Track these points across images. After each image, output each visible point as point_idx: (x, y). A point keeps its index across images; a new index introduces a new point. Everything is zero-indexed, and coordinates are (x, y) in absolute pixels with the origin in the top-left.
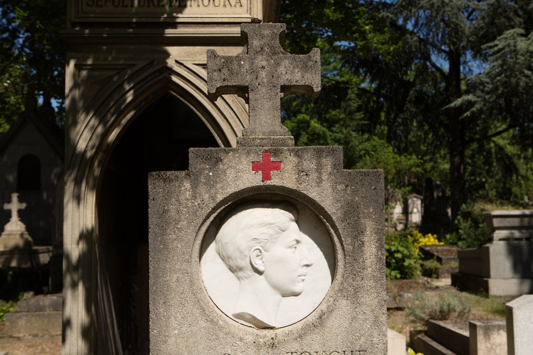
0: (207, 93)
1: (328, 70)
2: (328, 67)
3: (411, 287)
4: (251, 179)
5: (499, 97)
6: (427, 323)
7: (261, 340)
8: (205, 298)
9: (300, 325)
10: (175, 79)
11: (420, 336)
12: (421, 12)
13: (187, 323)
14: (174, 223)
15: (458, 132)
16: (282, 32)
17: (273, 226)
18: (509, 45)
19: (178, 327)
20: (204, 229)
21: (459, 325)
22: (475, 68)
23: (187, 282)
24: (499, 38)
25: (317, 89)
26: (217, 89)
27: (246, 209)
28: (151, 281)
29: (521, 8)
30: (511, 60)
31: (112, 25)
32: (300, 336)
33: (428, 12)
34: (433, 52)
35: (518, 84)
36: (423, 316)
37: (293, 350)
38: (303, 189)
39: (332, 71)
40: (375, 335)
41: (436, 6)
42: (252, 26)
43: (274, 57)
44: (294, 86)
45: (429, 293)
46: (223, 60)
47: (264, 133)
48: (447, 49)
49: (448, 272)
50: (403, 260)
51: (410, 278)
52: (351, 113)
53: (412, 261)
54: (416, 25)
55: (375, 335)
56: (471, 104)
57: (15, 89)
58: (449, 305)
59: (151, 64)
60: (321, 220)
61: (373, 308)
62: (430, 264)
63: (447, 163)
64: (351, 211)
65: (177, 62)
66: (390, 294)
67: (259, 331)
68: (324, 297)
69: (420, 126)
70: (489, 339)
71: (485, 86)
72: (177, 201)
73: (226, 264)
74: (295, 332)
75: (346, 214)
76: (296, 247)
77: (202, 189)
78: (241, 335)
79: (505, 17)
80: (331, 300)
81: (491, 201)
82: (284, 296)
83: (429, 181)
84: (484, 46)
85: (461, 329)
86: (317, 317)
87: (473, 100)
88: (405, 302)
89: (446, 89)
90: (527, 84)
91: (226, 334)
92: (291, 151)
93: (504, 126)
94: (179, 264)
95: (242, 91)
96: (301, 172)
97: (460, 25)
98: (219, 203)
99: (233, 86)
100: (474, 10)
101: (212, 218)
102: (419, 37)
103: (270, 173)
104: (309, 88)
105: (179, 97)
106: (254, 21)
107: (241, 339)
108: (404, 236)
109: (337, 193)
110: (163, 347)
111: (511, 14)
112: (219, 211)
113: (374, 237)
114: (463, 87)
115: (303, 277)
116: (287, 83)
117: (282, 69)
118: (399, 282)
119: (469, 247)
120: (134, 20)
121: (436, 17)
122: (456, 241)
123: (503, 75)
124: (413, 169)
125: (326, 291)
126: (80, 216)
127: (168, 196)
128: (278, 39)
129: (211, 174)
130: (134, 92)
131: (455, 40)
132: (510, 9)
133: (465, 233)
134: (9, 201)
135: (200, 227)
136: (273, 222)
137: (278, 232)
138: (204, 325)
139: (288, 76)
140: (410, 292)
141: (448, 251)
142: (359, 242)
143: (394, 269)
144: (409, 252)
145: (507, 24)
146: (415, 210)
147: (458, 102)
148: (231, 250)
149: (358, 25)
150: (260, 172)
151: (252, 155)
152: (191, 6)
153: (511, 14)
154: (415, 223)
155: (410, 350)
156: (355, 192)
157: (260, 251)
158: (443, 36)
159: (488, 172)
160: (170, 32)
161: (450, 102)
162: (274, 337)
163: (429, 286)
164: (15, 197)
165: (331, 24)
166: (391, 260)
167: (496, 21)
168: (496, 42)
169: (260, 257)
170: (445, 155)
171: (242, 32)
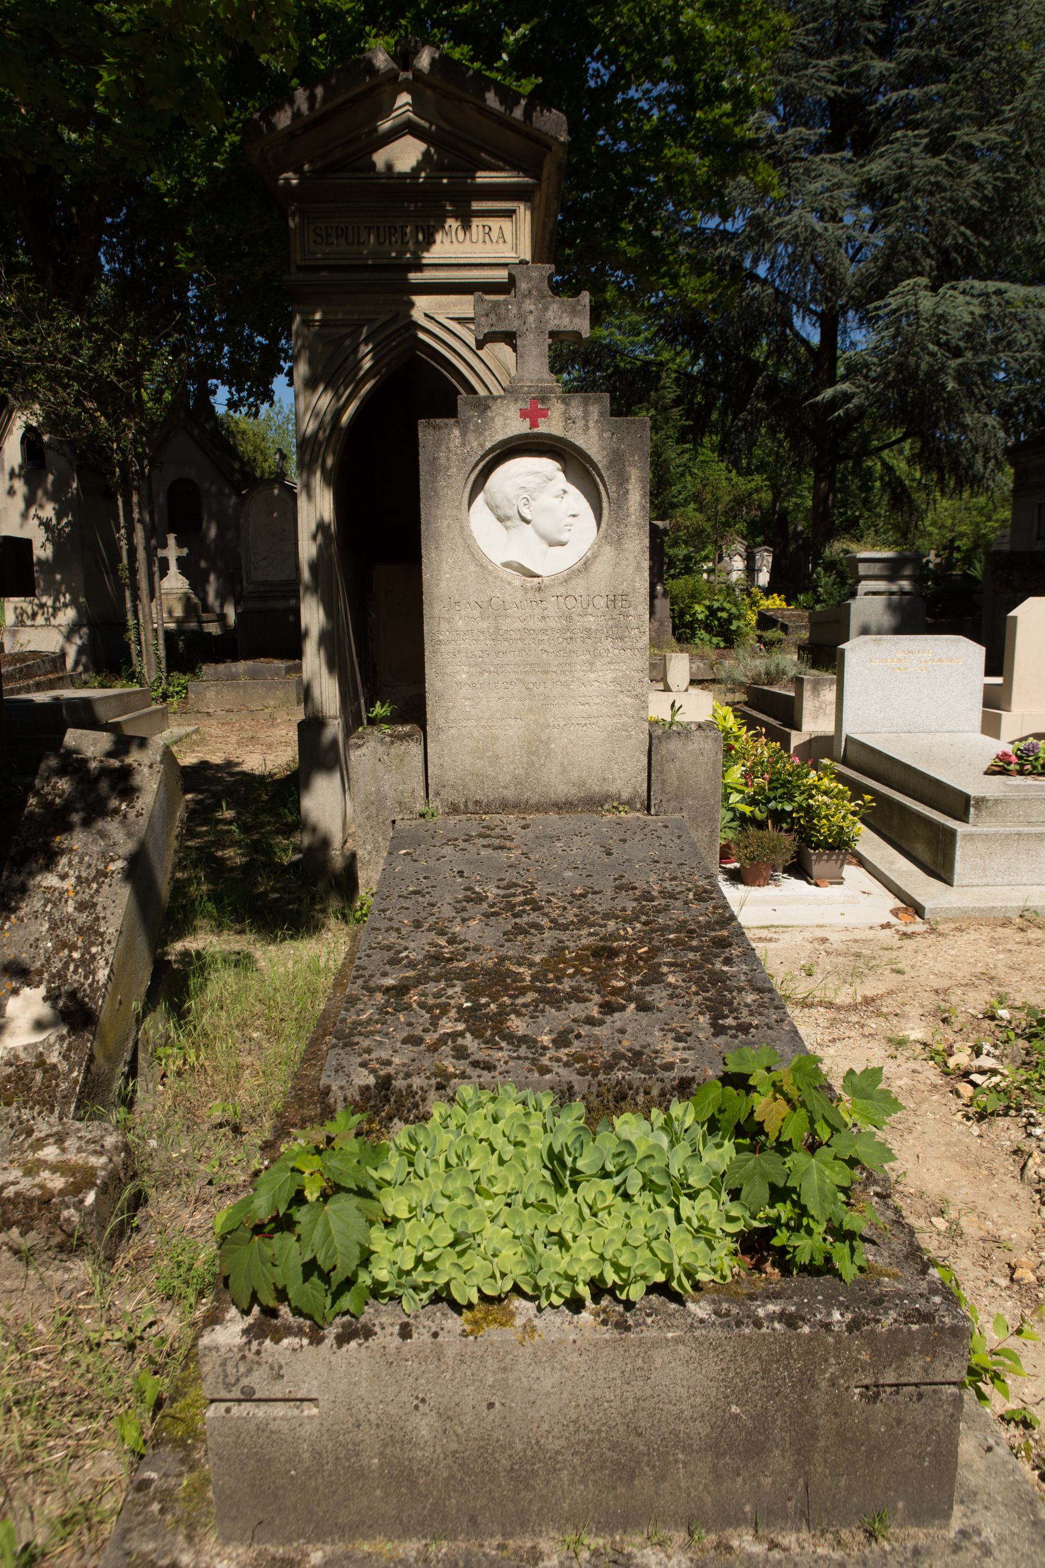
2: (636, 339)
4: (519, 427)
6: (750, 690)
10: (421, 336)
15: (829, 445)
18: (906, 303)
20: (473, 477)
22: (859, 339)
24: (891, 293)
28: (423, 527)
29: (934, 243)
35: (918, 366)
41: (802, 237)
42: (519, 268)
50: (729, 621)
52: (665, 409)
56: (847, 397)
59: (395, 318)
60: (587, 470)
64: (617, 459)
65: (426, 315)
69: (772, 431)
72: (447, 449)
75: (611, 462)
77: (471, 436)
79: (907, 258)
82: (551, 545)
89: (814, 374)
90: (931, 366)
92: (558, 398)
95: (509, 338)
96: (568, 419)
99: (501, 333)
104: (577, 334)
106: (523, 262)
107: (509, 583)
110: (435, 590)
113: (638, 485)
114: (841, 370)
117: (550, 314)
120: (370, 262)
127: (438, 443)
134: (164, 545)
146: (765, 569)
147: (828, 393)
148: (499, 499)
156: (620, 440)
160: (414, 277)
161: (818, 394)
164: (171, 539)
165: (629, 265)
171: (510, 275)
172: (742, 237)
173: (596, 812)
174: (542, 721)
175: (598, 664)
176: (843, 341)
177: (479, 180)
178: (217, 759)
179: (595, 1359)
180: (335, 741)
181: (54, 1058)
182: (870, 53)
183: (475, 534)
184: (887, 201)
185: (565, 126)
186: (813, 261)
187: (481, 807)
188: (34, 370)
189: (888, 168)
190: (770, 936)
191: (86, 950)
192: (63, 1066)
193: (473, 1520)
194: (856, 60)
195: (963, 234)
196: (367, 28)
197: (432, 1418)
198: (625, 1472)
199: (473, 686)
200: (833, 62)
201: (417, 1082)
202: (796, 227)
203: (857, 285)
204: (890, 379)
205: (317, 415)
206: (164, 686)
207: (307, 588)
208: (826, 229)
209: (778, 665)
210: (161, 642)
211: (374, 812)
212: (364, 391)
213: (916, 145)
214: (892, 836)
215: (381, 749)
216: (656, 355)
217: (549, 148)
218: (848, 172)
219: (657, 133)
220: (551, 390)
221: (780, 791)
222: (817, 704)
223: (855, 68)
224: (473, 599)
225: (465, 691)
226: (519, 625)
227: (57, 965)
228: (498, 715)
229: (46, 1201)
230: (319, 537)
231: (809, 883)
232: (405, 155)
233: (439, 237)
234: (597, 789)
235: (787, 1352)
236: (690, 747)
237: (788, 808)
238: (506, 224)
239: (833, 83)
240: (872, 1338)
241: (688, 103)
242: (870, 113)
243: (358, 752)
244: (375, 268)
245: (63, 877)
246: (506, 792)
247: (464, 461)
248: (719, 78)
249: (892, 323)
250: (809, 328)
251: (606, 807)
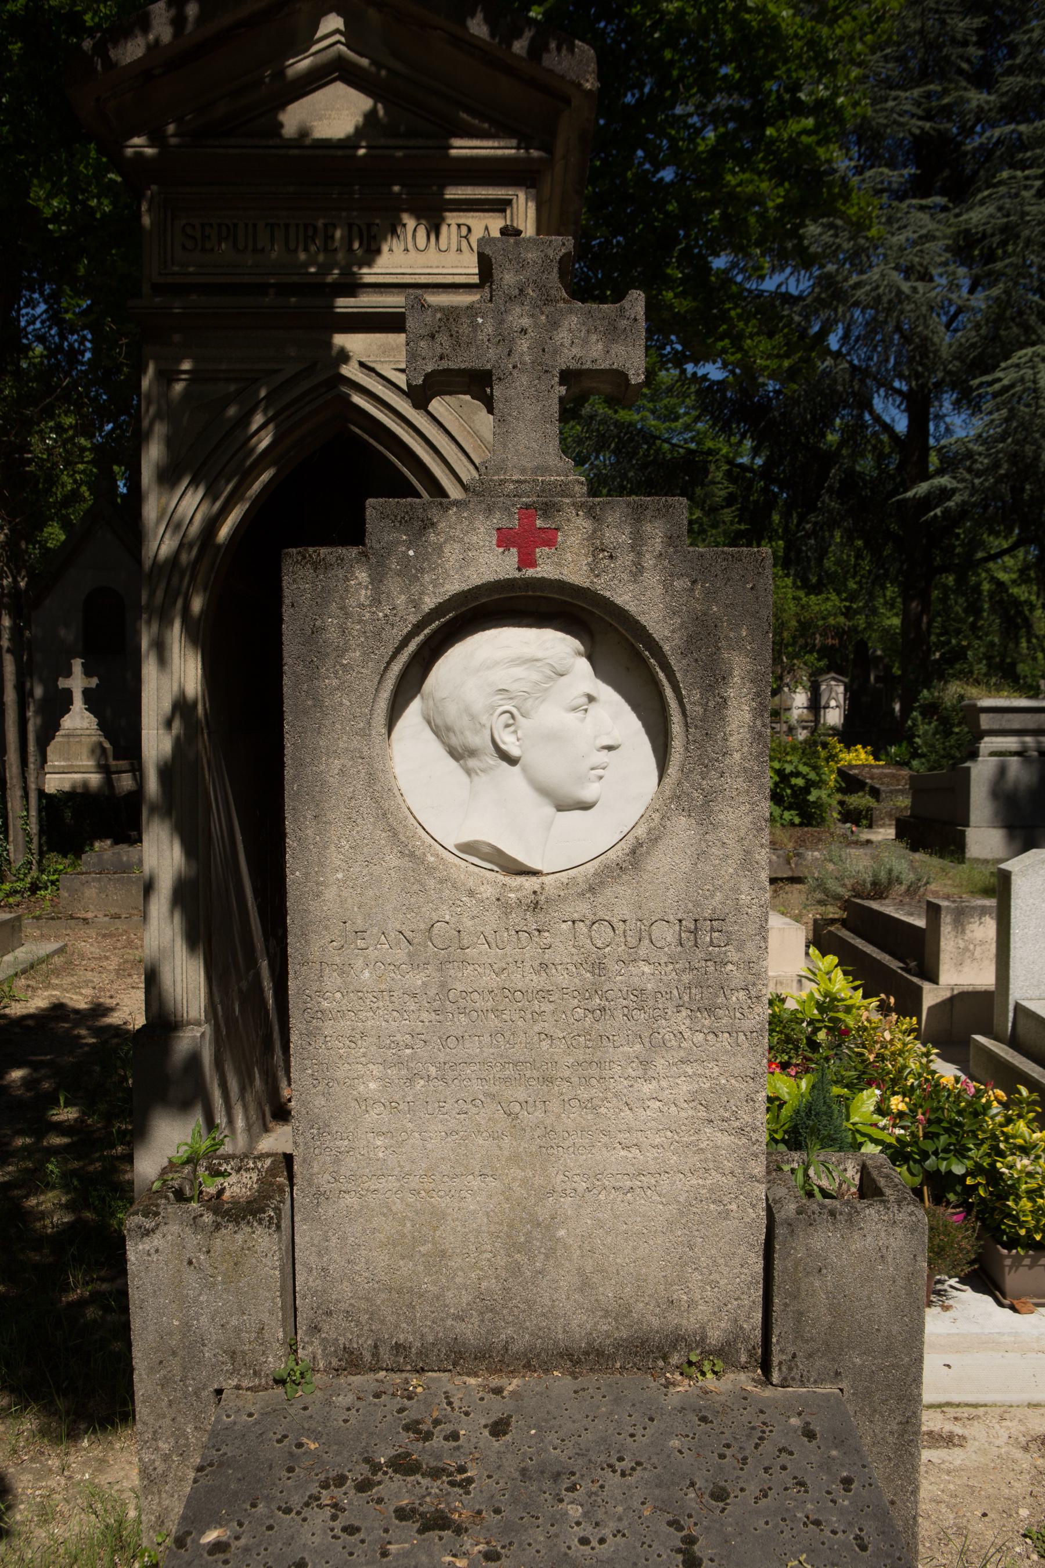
0: (405, 388)
1: (673, 430)
2: (673, 425)
3: (820, 840)
6: (847, 905)
7: (512, 895)
8: (399, 808)
9: (591, 868)
10: (358, 400)
11: (832, 929)
12: (857, 313)
13: (361, 858)
14: (335, 654)
15: (918, 549)
16: (565, 255)
17: (539, 664)
18: (1022, 380)
19: (344, 865)
20: (397, 667)
21: (907, 908)
22: (958, 426)
23: (362, 775)
24: (1003, 365)
26: (428, 376)
27: (484, 630)
28: (289, 773)
30: (1027, 410)
32: (591, 889)
33: (870, 312)
34: (877, 391)
36: (840, 890)
37: (576, 916)
38: (603, 586)
39: (681, 433)
40: (745, 888)
41: (885, 299)
43: (546, 310)
44: (589, 371)
45: (854, 851)
46: (439, 316)
47: (523, 471)
48: (905, 388)
49: (890, 815)
50: (806, 790)
51: (818, 825)
52: (714, 510)
53: (823, 794)
54: (846, 337)
55: (745, 888)
56: (945, 494)
57: (66, 451)
58: (890, 871)
61: (742, 835)
62: (858, 800)
63: (897, 615)
64: (702, 635)
65: (362, 364)
66: (780, 852)
67: (507, 879)
68: (642, 812)
69: (849, 538)
70: (963, 932)
71: (975, 461)
72: (344, 608)
73: (443, 743)
74: (580, 880)
76: (586, 710)
77: (393, 585)
78: (471, 883)
79: (1017, 325)
80: (657, 816)
81: (977, 682)
82: (560, 808)
83: (862, 646)
84: (975, 382)
85: (911, 914)
86: (627, 851)
87: (949, 486)
88: (806, 866)
89: (900, 468)
91: (441, 882)
92: (578, 506)
94: (345, 738)
95: (478, 384)
96: (600, 551)
97: (931, 340)
98: (428, 614)
100: (960, 311)
101: (412, 646)
102: (850, 362)
103: (534, 553)
105: (366, 437)
107: (471, 893)
108: (809, 750)
109: (673, 596)
110: (313, 906)
112: (427, 631)
114: (934, 460)
115: (600, 772)
116: (573, 365)
117: (563, 336)
118: (798, 832)
119: (930, 770)
121: (886, 322)
122: (907, 757)
123: (1010, 440)
124: (831, 621)
125: (646, 800)
126: (173, 675)
128: (556, 270)
129: (411, 553)
130: (276, 427)
131: (920, 369)
132: (1031, 308)
133: (925, 743)
134: (69, 674)
135: (389, 663)
136: (540, 654)
137: (550, 678)
138: (396, 862)
139: (575, 351)
140: (818, 850)
141: (893, 776)
142: (717, 699)
143: (788, 809)
144: (818, 774)
145: (1023, 339)
147: (922, 488)
148: (452, 713)
150: (514, 550)
151: (498, 515)
152: (391, 250)
154: (833, 728)
155: (812, 950)
156: (710, 596)
157: (513, 717)
158: (897, 363)
160: (344, 304)
161: (906, 491)
162: (539, 891)
163: (854, 838)
164: (77, 665)
166: (783, 789)
167: (1002, 333)
168: (999, 374)
169: (512, 729)
170: (893, 599)
172: (809, 301)
173: (651, 1370)
174: (538, 1181)
175: (660, 1063)
176: (937, 427)
177: (453, 152)
178: (79, 1001)
180: (194, 1060)
182: (964, 84)
183: (403, 783)
184: (990, 257)
185: (593, 66)
186: (898, 328)
189: (991, 216)
190: (948, 1427)
194: (946, 92)
199: (393, 1106)
200: (916, 92)
202: (878, 287)
203: (955, 358)
204: (1002, 472)
205: (178, 526)
206: (34, 873)
207: (153, 810)
208: (915, 290)
209: (890, 871)
210: (33, 813)
211: (177, 1370)
212: (257, 486)
213: (1027, 188)
215: (193, 1239)
216: (698, 444)
217: (567, 101)
218: (939, 222)
219: (716, 154)
220: (564, 490)
221: (944, 1139)
222: (962, 944)
223: (946, 101)
224: (393, 925)
225: (374, 1116)
226: (489, 980)
228: (445, 1168)
230: (177, 724)
231: (1001, 1305)
232: (335, 114)
234: (656, 1323)
236: (857, 1245)
237: (958, 1169)
239: (920, 118)
241: (754, 121)
242: (966, 153)
243: (145, 1245)
244: (285, 290)
246: (460, 1327)
247: (378, 635)
248: (796, 87)
249: (1004, 403)
250: (894, 412)
251: (675, 1359)
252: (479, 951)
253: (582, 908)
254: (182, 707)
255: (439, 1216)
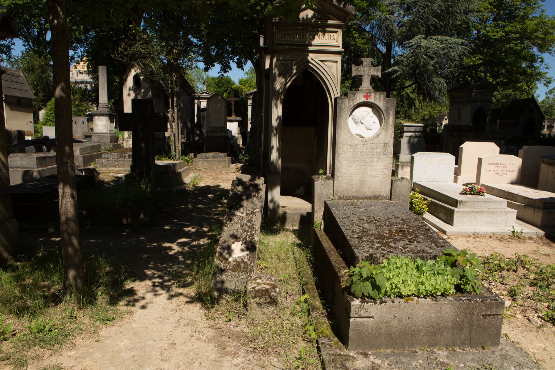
5: (410, 68)
10: (310, 65)
25: (380, 77)
31: (289, 45)
35: (420, 62)
48: (386, 41)
56: (396, 71)
59: (303, 59)
64: (387, 109)
77: (351, 101)
93: (411, 83)
96: (376, 98)
111: (420, 26)
117: (371, 71)
127: (342, 103)
147: (390, 70)
148: (356, 118)
149: (352, 33)
153: (420, 26)
159: (402, 106)
160: (310, 48)
168: (411, 41)
179: (431, 308)
181: (246, 260)
187: (347, 198)
188: (147, 57)
191: (251, 232)
192: (249, 262)
193: (402, 345)
195: (435, 21)
196: (494, 100)
197: (397, 321)
198: (434, 333)
199: (347, 166)
201: (378, 255)
210: (180, 145)
214: (432, 212)
215: (323, 182)
225: (345, 167)
226: (360, 150)
227: (244, 236)
229: (267, 290)
230: (278, 121)
233: (316, 37)
235: (469, 307)
238: (335, 35)
240: (486, 303)
245: (242, 213)
250: (383, 47)
252: (359, 147)
253: (371, 142)
254: (278, 117)
255: (352, 180)
